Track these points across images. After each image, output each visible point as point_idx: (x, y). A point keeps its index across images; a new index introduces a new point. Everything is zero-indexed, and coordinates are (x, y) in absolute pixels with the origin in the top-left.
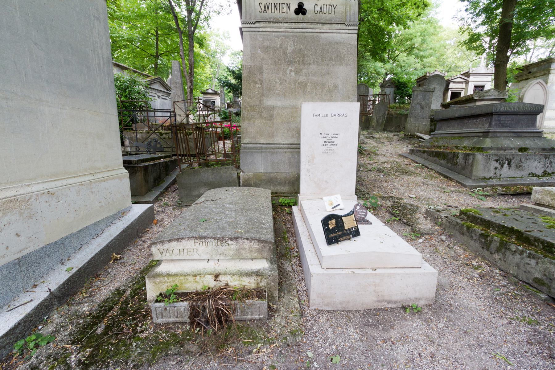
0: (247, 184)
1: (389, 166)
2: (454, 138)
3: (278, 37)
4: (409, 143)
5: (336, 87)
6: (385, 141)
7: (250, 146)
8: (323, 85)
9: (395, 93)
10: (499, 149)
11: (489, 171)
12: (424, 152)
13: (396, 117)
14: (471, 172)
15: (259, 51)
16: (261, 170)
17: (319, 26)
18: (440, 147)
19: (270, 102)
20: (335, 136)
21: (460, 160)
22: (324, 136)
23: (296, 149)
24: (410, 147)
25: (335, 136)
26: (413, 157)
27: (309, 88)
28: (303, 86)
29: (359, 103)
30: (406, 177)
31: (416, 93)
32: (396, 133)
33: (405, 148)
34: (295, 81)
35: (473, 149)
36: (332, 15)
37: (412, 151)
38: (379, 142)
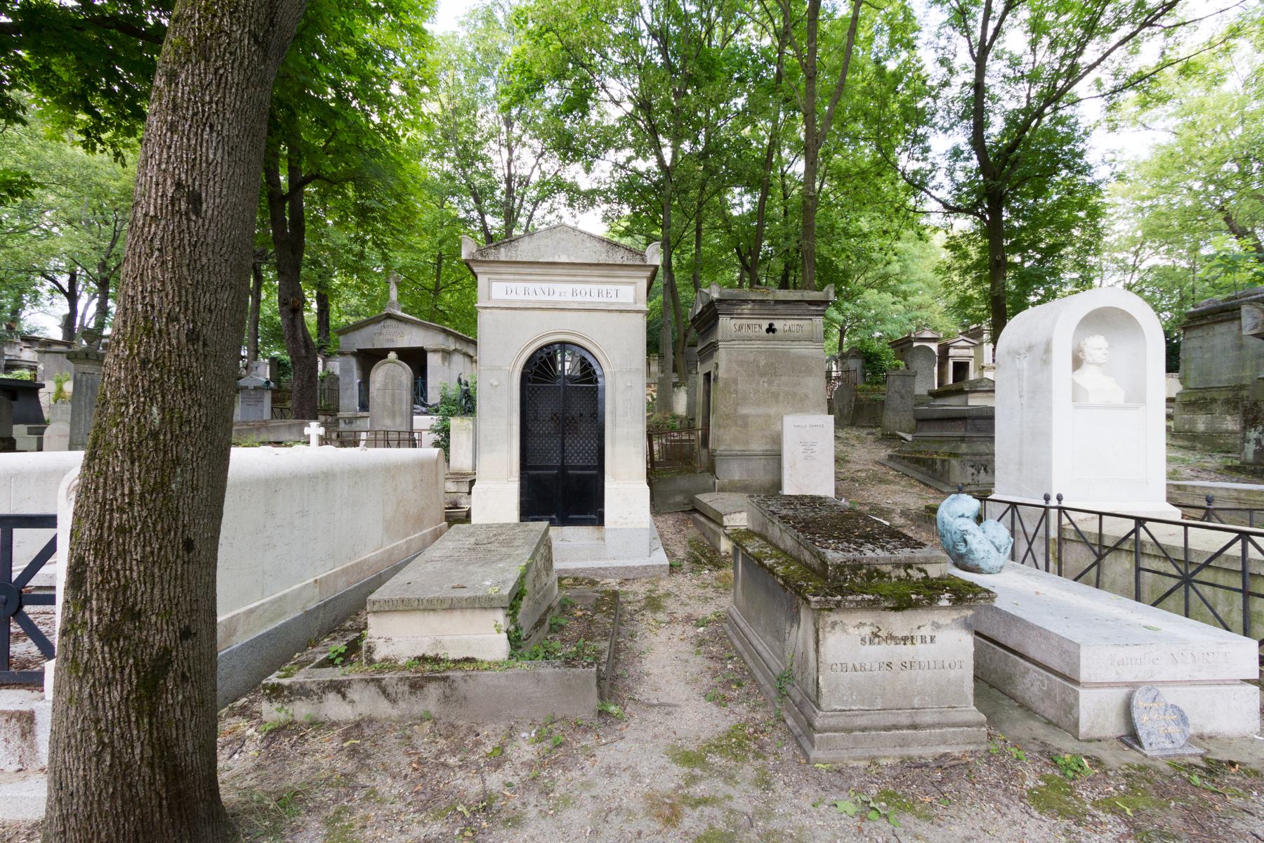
0: (722, 490)
1: (864, 475)
2: (935, 441)
3: (751, 352)
4: (889, 446)
5: (806, 396)
6: (855, 442)
7: (726, 453)
8: (795, 395)
9: (863, 367)
10: (974, 455)
11: (966, 477)
12: (904, 458)
13: (869, 405)
14: (949, 478)
15: (734, 365)
16: (737, 478)
17: (789, 342)
18: (920, 452)
19: (744, 410)
20: (813, 444)
21: (938, 466)
22: (804, 444)
23: (776, 457)
24: (889, 451)
25: (813, 444)
26: (892, 464)
27: (781, 398)
28: (776, 396)
29: (832, 417)
30: (883, 487)
31: (891, 378)
32: (871, 430)
33: (883, 452)
34: (768, 391)
35: (950, 454)
36: (800, 333)
37: (891, 457)
38: (847, 445)
